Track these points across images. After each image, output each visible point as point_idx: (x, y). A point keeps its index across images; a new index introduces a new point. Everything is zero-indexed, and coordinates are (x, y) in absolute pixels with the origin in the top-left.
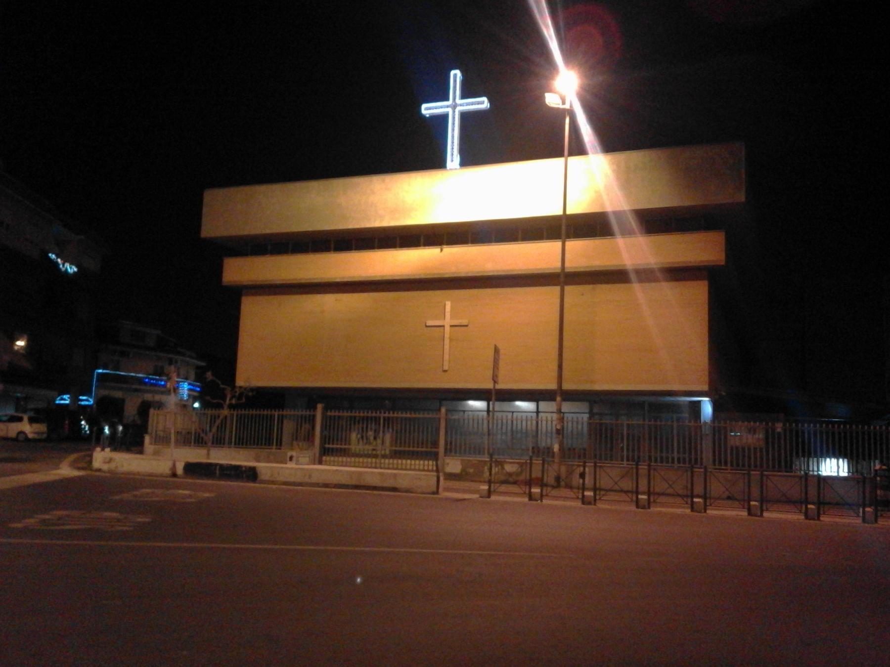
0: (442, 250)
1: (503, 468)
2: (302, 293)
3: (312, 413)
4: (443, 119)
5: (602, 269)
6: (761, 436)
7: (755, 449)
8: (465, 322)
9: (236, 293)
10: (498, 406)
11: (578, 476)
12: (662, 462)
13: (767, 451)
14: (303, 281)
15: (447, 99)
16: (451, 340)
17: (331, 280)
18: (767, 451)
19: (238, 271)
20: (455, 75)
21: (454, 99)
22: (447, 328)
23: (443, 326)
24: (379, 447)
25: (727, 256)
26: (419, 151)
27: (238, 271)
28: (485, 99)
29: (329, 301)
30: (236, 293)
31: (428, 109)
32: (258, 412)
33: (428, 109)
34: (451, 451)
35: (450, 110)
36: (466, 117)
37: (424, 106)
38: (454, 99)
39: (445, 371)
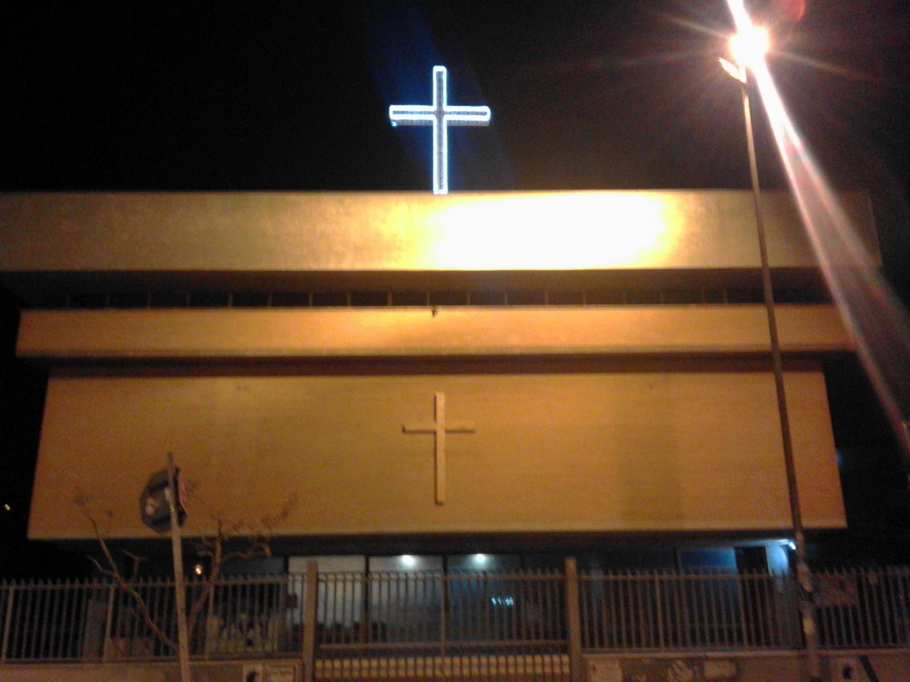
0: (434, 313)
1: (702, 672)
2: (109, 375)
3: (169, 583)
4: (422, 132)
5: (667, 350)
6: (852, 590)
7: (845, 609)
8: (469, 424)
9: (38, 374)
10: (377, 564)
11: (840, 675)
12: (529, 638)
13: (864, 612)
14: (182, 354)
15: (429, 102)
16: (448, 453)
17: (235, 354)
18: (864, 612)
19: (44, 333)
20: (440, 74)
21: (440, 104)
22: (441, 434)
23: (435, 433)
24: (258, 641)
25: (46, 384)
26: (397, 167)
27: (44, 333)
28: (486, 109)
29: (226, 389)
30: (38, 374)
31: (401, 114)
32: (32, 586)
33: (401, 114)
34: (592, 644)
35: (433, 118)
36: (457, 133)
37: (393, 108)
38: (440, 104)
39: (437, 503)
